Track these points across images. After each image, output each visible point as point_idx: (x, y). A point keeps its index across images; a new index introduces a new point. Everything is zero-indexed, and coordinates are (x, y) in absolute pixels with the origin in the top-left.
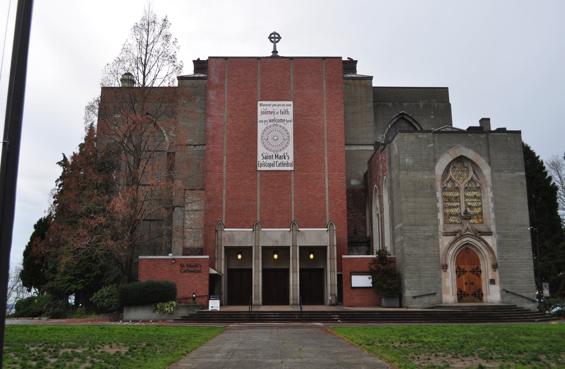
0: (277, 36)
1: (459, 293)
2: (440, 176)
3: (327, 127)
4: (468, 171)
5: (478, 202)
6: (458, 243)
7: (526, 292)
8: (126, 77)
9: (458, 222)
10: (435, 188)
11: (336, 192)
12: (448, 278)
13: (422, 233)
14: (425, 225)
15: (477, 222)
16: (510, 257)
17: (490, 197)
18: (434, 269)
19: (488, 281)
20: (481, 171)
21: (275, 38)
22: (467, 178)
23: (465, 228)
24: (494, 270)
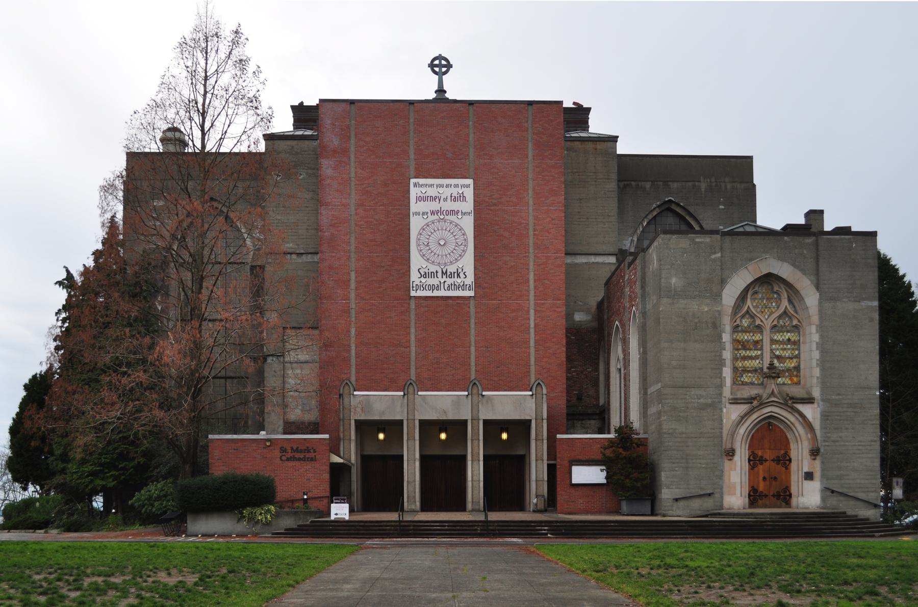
0: (444, 62)
1: (752, 494)
2: (731, 306)
3: (534, 223)
4: (780, 299)
6: (754, 416)
8: (169, 134)
9: (756, 382)
10: (720, 327)
11: (549, 332)
13: (695, 399)
14: (699, 387)
15: (789, 382)
16: (841, 437)
18: (712, 457)
20: (801, 299)
21: (440, 66)
22: (776, 311)
23: (769, 391)
24: (813, 457)
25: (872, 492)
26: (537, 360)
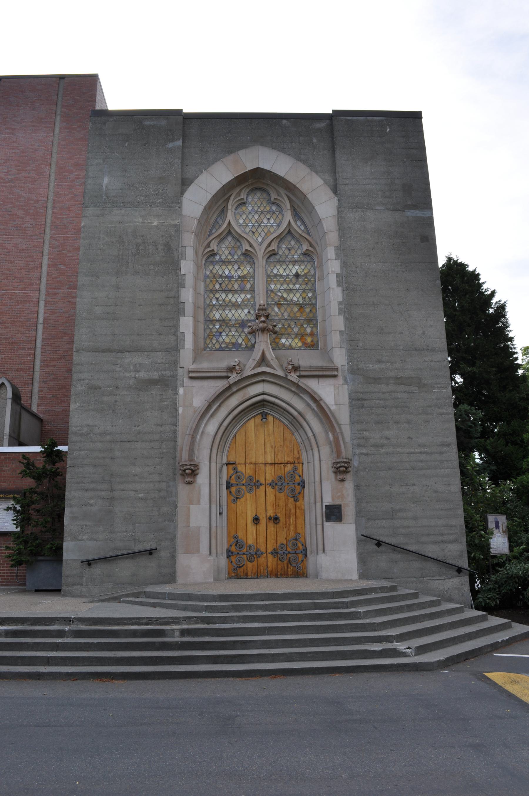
2: (194, 218)
3: (54, 200)
4: (281, 212)
5: (304, 290)
6: (234, 401)
7: (435, 543)
11: (60, 328)
12: (199, 502)
13: (130, 371)
14: (138, 350)
16: (388, 439)
17: (333, 272)
19: (319, 512)
20: (311, 209)
24: (340, 477)
25: (450, 542)
26: (45, 364)
